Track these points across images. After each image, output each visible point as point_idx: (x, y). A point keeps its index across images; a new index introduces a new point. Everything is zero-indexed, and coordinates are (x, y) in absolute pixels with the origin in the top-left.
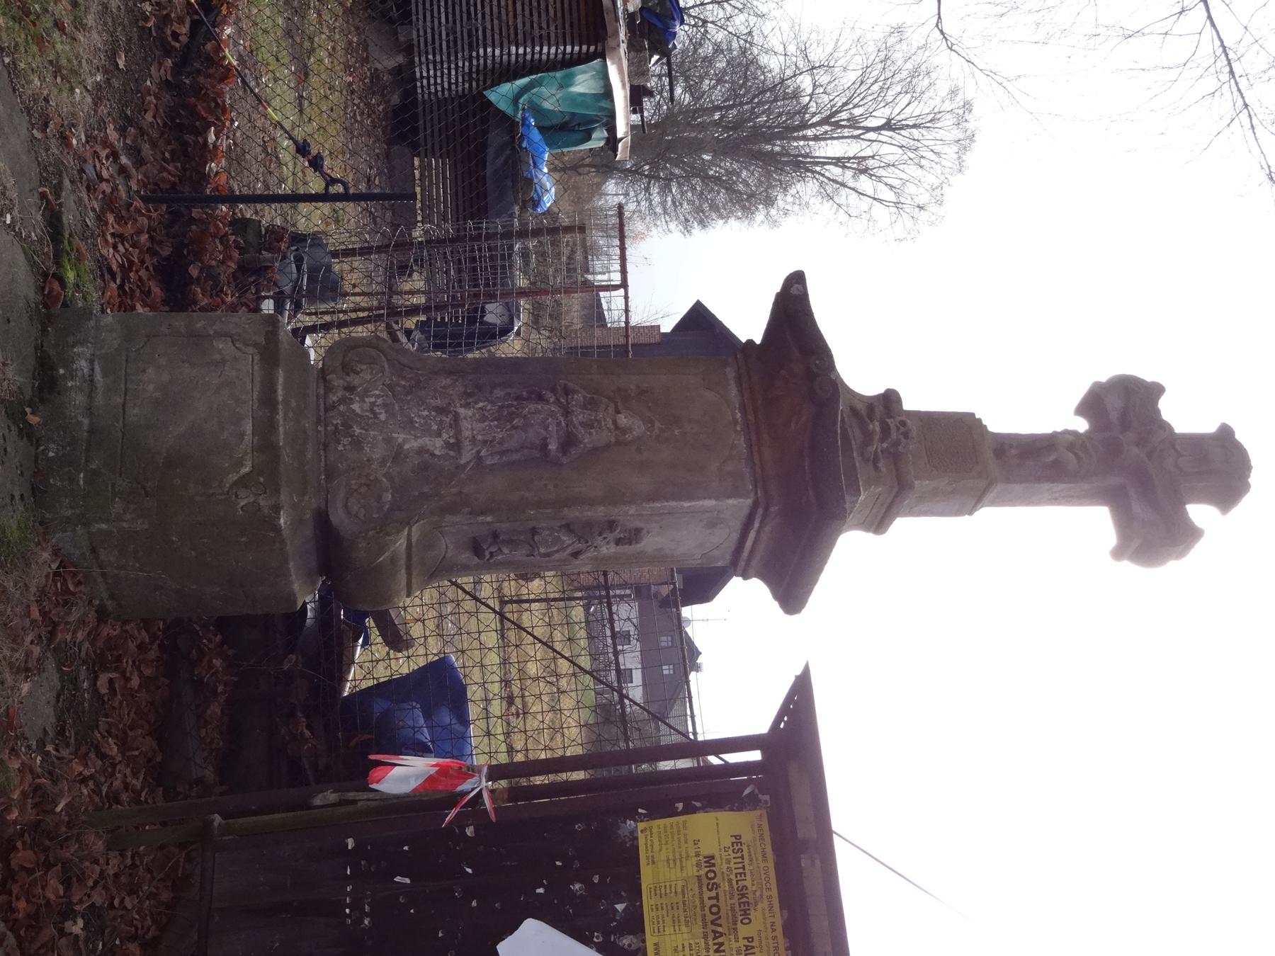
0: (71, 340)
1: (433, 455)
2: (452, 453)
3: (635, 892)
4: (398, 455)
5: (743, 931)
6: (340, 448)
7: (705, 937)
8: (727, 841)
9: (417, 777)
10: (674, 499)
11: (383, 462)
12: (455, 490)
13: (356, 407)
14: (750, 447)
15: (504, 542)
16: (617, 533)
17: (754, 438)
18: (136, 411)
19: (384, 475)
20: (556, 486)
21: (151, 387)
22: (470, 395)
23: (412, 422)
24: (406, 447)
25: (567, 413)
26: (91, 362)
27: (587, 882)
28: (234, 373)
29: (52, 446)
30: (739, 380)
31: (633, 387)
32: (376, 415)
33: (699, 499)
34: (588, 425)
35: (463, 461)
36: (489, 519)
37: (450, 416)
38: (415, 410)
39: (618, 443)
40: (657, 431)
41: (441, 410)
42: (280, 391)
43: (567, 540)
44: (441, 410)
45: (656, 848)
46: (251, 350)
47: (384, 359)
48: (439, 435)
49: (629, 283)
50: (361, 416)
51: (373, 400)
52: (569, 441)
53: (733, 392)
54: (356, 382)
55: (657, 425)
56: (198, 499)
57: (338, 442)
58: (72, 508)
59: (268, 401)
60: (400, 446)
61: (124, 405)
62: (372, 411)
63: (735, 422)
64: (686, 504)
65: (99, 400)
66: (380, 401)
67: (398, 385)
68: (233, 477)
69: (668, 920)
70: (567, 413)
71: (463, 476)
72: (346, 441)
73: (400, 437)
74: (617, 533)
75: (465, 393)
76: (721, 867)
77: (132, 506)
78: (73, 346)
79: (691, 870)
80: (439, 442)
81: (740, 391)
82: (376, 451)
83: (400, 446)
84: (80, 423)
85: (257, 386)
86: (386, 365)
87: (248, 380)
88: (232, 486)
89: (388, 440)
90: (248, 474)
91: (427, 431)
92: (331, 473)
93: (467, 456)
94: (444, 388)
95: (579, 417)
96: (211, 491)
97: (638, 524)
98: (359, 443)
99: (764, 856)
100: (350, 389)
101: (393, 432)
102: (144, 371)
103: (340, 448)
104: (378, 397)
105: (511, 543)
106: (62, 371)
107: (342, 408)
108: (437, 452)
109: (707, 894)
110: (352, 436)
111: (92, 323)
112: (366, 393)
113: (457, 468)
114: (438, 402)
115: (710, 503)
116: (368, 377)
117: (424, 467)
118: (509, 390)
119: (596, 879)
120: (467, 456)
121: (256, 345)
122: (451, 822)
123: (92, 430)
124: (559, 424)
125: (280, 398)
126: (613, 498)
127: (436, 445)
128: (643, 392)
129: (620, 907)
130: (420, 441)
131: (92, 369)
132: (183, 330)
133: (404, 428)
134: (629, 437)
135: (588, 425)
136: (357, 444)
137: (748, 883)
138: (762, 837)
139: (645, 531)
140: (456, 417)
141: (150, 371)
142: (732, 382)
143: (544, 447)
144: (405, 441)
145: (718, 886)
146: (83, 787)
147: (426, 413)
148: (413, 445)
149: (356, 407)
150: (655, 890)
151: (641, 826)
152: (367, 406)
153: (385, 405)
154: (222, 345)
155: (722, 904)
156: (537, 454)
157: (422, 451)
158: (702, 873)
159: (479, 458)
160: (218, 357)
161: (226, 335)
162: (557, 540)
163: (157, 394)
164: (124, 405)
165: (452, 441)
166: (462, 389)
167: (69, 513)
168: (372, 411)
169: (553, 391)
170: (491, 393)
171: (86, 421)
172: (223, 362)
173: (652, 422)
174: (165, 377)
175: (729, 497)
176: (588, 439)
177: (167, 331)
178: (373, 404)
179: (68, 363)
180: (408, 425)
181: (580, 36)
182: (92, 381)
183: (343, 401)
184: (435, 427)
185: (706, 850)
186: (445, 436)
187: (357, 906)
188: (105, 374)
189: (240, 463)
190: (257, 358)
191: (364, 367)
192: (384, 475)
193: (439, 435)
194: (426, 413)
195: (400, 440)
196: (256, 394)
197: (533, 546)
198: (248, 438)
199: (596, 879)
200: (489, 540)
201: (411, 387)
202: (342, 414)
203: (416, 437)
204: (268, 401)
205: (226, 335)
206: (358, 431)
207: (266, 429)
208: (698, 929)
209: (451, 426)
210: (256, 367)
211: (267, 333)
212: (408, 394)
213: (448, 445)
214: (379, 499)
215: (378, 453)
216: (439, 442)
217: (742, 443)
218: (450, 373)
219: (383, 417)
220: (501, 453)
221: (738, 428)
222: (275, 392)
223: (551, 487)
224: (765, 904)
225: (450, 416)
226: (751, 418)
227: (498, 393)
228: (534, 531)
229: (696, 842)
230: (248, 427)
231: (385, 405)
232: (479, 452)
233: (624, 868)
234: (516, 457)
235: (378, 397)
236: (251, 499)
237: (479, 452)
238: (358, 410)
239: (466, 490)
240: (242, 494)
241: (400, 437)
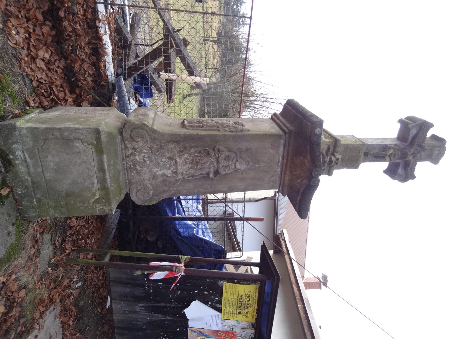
0: (10, 141)
1: (167, 176)
2: (174, 175)
3: (221, 296)
4: (154, 177)
5: (246, 310)
6: (133, 174)
7: (237, 309)
8: (247, 292)
11: (149, 180)
12: (175, 189)
13: (137, 157)
14: (282, 171)
17: (284, 169)
18: (48, 174)
19: (150, 184)
20: (211, 187)
21: (52, 164)
22: (181, 152)
23: (159, 164)
24: (157, 174)
25: (218, 162)
26: (23, 152)
27: (209, 292)
28: (85, 157)
29: (18, 189)
30: (284, 145)
31: (244, 147)
32: (145, 162)
37: (174, 161)
38: (160, 159)
40: (250, 166)
41: (170, 158)
42: (106, 164)
44: (170, 158)
45: (228, 289)
46: (90, 146)
47: (147, 135)
48: (170, 169)
49: (252, 17)
50: (140, 162)
51: (144, 154)
52: (217, 173)
53: (281, 150)
54: (136, 146)
55: (251, 163)
56: (81, 208)
57: (132, 172)
58: (35, 213)
59: (102, 169)
60: (155, 173)
61: (43, 172)
62: (144, 160)
63: (279, 162)
65: (32, 170)
66: (146, 156)
67: (153, 147)
68: (92, 200)
69: (228, 306)
70: (218, 162)
71: (178, 184)
72: (135, 172)
73: (155, 170)
75: (180, 151)
76: (244, 298)
77: (57, 211)
78: (13, 144)
79: (236, 297)
80: (169, 172)
81: (284, 149)
82: (146, 176)
83: (155, 173)
84: (27, 180)
85: (96, 164)
86: (148, 139)
87: (92, 160)
88: (93, 203)
89: (151, 171)
90: (98, 198)
91: (165, 167)
92: (130, 183)
94: (172, 148)
95: (223, 163)
96: (86, 205)
98: (139, 173)
99: (255, 297)
100: (134, 149)
102: (47, 157)
103: (133, 174)
104: (146, 153)
106: (11, 157)
107: (132, 158)
108: (169, 175)
109: (239, 303)
110: (137, 170)
111: (17, 133)
112: (140, 152)
113: (176, 181)
114: (169, 155)
116: (141, 144)
117: (164, 181)
118: (196, 149)
119: (211, 292)
120: (180, 177)
121: (92, 144)
122: (173, 288)
123: (33, 182)
124: (214, 166)
125: (106, 168)
127: (169, 173)
128: (248, 150)
129: (216, 298)
130: (162, 171)
131: (24, 155)
132: (59, 136)
133: (156, 167)
135: (225, 167)
136: (139, 173)
137: (250, 303)
138: (256, 292)
140: (176, 162)
141: (49, 156)
142: (282, 146)
143: (208, 174)
144: (157, 171)
145: (242, 302)
146: (68, 101)
147: (164, 160)
148: (160, 173)
149: (137, 157)
150: (226, 299)
151: (224, 283)
152: (141, 157)
153: (148, 157)
154: (78, 144)
155: (242, 305)
157: (163, 175)
158: (239, 298)
160: (77, 150)
161: (79, 139)
163: (55, 167)
164: (43, 172)
165: (174, 171)
166: (178, 149)
167: (34, 214)
168: (144, 160)
169: (214, 150)
170: (190, 150)
171: (29, 179)
172: (80, 152)
173: (249, 162)
174: (57, 160)
177: (52, 137)
178: (144, 157)
179: (13, 153)
180: (158, 165)
182: (26, 161)
183: (132, 154)
184: (168, 166)
185: (240, 293)
186: (172, 169)
187: (149, 286)
188: (31, 158)
189: (94, 195)
190: (94, 150)
191: (139, 139)
192: (150, 184)
193: (170, 169)
194: (164, 160)
195: (155, 171)
196: (96, 166)
198: (96, 185)
199: (211, 292)
201: (159, 149)
202: (132, 161)
203: (161, 170)
204: (102, 169)
205: (79, 139)
206: (138, 168)
207: (102, 181)
208: (236, 308)
209: (174, 165)
210: (94, 155)
211: (96, 137)
212: (158, 151)
213: (173, 172)
214: (148, 193)
215: (147, 176)
216: (169, 172)
217: (279, 170)
218: (174, 142)
219: (148, 162)
221: (279, 164)
222: (104, 165)
223: (209, 187)
224: (253, 307)
225: (174, 161)
226: (285, 161)
227: (193, 150)
229: (238, 291)
230: (95, 181)
231: (148, 157)
233: (220, 291)
235: (146, 153)
236: (101, 207)
238: (138, 159)
239: (179, 189)
240: (97, 206)
241: (155, 170)
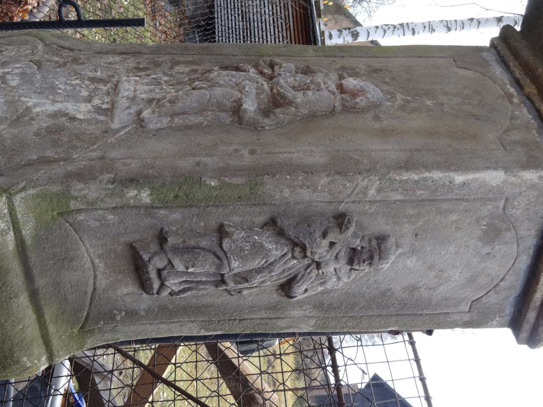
2: (102, 118)
9: (530, 248)
10: (439, 166)
15: (176, 250)
16: (350, 238)
33: (477, 169)
34: (303, 88)
35: (115, 125)
36: (145, 196)
39: (347, 109)
43: (275, 249)
52: (276, 102)
55: (399, 96)
64: (459, 178)
74: (350, 238)
93: (122, 118)
97: (379, 225)
101: (23, 95)
105: (188, 251)
115: (494, 177)
126: (343, 167)
127: (82, 110)
134: (361, 101)
139: (391, 241)
156: (226, 118)
159: (140, 122)
162: (258, 249)
175: (525, 167)
176: (312, 231)
181: (303, 41)
197: (220, 256)
200: (154, 247)
216: (85, 107)
220: (173, 115)
228: (221, 232)
232: (139, 113)
234: (193, 119)
237: (139, 113)
